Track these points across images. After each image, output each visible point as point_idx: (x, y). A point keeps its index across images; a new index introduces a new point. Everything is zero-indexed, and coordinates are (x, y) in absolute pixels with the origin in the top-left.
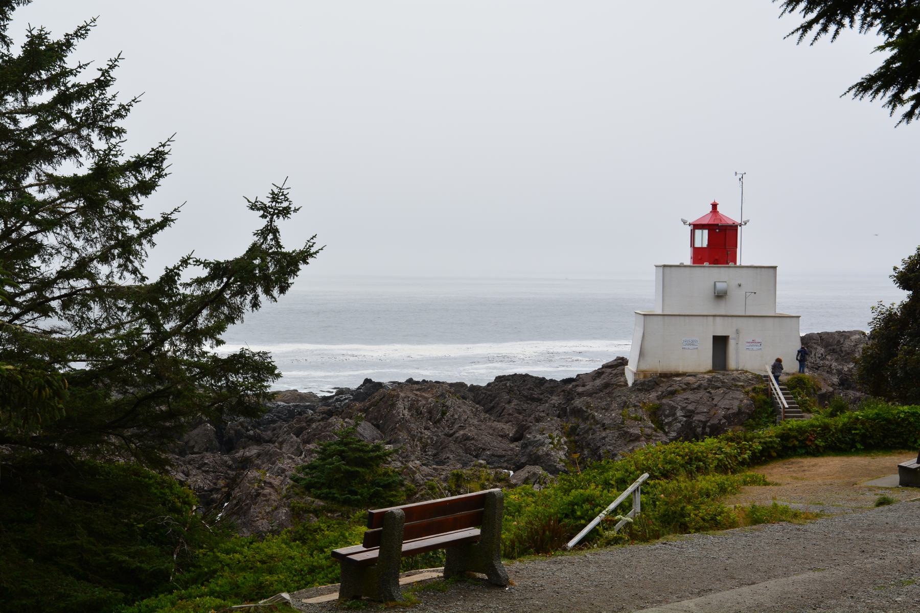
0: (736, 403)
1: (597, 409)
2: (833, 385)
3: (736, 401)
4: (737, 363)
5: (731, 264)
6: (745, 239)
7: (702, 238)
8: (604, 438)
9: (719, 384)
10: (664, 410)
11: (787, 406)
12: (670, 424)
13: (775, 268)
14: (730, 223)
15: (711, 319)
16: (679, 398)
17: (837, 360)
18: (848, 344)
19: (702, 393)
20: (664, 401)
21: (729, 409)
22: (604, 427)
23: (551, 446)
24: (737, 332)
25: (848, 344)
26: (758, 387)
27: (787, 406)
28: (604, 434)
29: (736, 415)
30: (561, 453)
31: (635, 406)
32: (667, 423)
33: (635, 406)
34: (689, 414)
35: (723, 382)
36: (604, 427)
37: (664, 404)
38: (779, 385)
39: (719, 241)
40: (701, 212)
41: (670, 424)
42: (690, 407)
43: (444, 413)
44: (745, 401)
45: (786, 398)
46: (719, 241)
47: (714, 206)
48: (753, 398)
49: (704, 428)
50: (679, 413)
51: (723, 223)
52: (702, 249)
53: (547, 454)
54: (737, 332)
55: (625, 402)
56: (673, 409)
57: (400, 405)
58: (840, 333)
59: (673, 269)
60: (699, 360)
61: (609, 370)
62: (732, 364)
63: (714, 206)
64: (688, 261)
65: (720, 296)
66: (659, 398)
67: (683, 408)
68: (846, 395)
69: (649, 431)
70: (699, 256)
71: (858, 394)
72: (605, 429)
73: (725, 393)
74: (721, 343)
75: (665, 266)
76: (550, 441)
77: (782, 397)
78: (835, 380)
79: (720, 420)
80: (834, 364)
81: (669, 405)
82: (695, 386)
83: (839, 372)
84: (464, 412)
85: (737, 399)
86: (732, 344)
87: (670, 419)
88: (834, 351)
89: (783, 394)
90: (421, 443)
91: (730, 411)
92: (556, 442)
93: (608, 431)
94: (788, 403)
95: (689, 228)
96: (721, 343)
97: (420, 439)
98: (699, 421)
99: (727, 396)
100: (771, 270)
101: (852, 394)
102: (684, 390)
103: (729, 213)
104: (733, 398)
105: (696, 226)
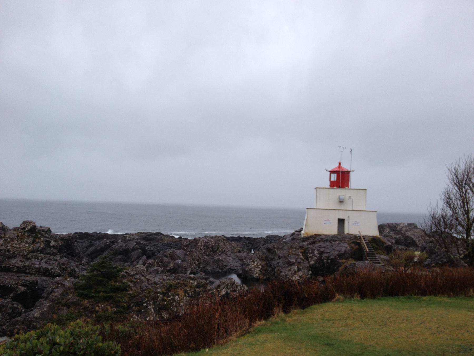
0: (344, 248)
1: (278, 249)
2: (392, 243)
3: (345, 247)
4: (349, 230)
5: (347, 188)
6: (352, 176)
7: (334, 177)
8: (278, 263)
9: (337, 239)
10: (309, 251)
11: (368, 251)
12: (311, 257)
13: (366, 190)
14: (346, 170)
15: (337, 211)
16: (317, 245)
17: (394, 234)
18: (398, 228)
19: (328, 243)
20: (309, 246)
21: (340, 251)
22: (280, 258)
23: (253, 266)
24: (349, 217)
25: (398, 228)
26: (356, 240)
27: (368, 251)
28: (278, 261)
29: (343, 254)
30: (258, 269)
31: (295, 248)
32: (310, 257)
33: (295, 248)
34: (321, 253)
35: (338, 239)
36: (280, 258)
37: (309, 248)
38: (365, 240)
39: (341, 179)
40: (334, 166)
41: (311, 257)
42: (322, 250)
43: (218, 249)
44: (348, 248)
45: (368, 247)
46: (341, 179)
47: (340, 164)
48: (352, 247)
49: (327, 260)
50: (316, 252)
51: (343, 170)
52: (334, 181)
53: (250, 270)
54: (349, 217)
55: (291, 246)
56: (313, 250)
57: (200, 244)
58: (396, 224)
59: (362, 212)
60: (332, 230)
61: (297, 233)
62: (346, 232)
63: (340, 164)
64: (328, 186)
65: (341, 202)
66: (308, 245)
67: (318, 250)
68: (398, 247)
69: (299, 260)
70: (333, 184)
71: (403, 247)
72: (280, 259)
73: (339, 244)
74: (341, 222)
75: (317, 188)
76: (253, 263)
77: (366, 246)
78: (394, 241)
79: (335, 256)
80: (393, 235)
81: (311, 248)
82: (325, 240)
83: (395, 238)
84: (227, 248)
85: (344, 246)
86: (346, 222)
87: (311, 255)
88: (393, 230)
89: (367, 245)
90: (198, 261)
91: (341, 252)
92: (255, 264)
93: (281, 259)
94: (369, 250)
95: (329, 173)
96: (341, 222)
97: (198, 260)
98: (326, 257)
99: (339, 245)
100: (364, 191)
101: (400, 247)
102: (319, 241)
103: (346, 167)
104: (343, 246)
105: (332, 172)
